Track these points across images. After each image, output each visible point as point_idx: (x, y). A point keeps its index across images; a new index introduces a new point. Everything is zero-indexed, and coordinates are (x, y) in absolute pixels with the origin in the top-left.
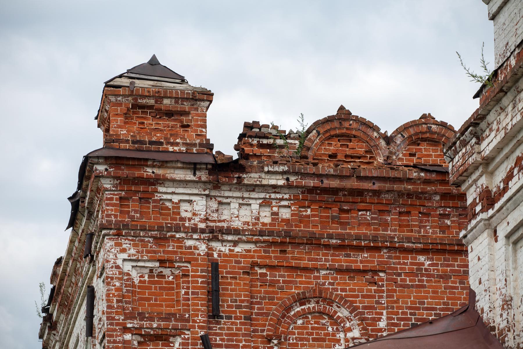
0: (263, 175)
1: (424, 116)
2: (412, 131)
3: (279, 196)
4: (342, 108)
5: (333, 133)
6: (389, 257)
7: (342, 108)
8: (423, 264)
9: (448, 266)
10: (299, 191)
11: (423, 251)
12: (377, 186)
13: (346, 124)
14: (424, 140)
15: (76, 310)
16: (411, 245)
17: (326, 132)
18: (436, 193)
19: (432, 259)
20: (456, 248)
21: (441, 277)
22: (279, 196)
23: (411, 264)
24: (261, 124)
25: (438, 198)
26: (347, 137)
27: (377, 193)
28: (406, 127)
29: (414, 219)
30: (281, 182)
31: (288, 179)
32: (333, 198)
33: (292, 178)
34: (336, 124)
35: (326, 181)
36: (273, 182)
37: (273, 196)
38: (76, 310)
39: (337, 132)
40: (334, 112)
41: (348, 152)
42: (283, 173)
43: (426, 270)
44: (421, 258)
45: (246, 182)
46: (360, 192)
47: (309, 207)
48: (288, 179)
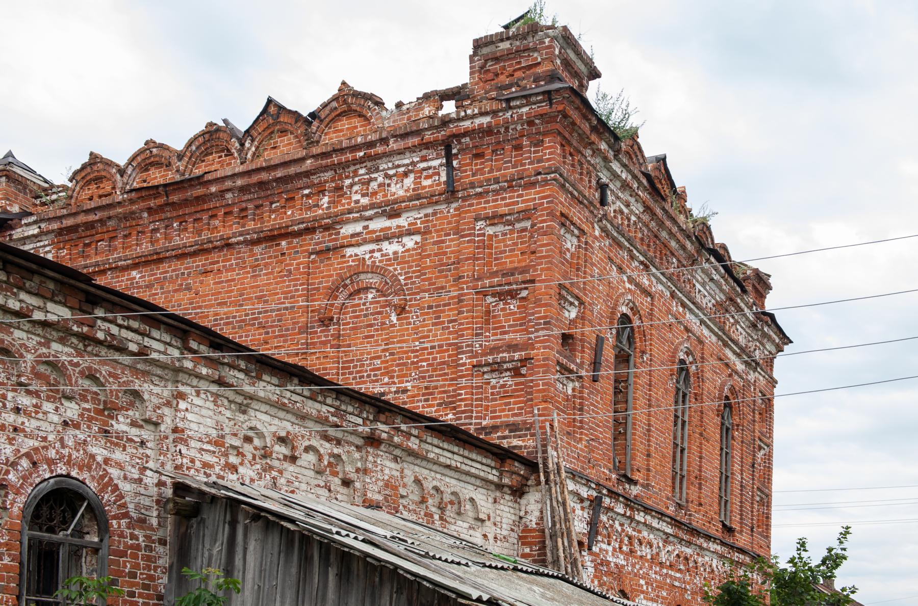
0: (24, 228)
1: (147, 143)
2: (139, 159)
3: (42, 244)
4: (91, 154)
5: (88, 178)
6: (112, 278)
7: (91, 154)
8: (135, 278)
9: (153, 275)
10: (52, 236)
11: (135, 266)
12: (99, 215)
13: (95, 168)
14: (152, 164)
15: (712, 326)
16: (123, 263)
17: (83, 178)
18: (142, 211)
19: (141, 272)
20: (155, 257)
21: (147, 286)
22: (42, 244)
23: (128, 280)
24: (639, 140)
25: (145, 215)
26: (98, 179)
27: (102, 221)
28: (134, 158)
29: (133, 240)
30: (36, 231)
31: (40, 227)
32: (74, 236)
33: (43, 225)
34: (89, 170)
35: (64, 222)
36: (31, 233)
37: (38, 244)
38: (712, 326)
39: (92, 176)
40: (86, 159)
41: (101, 192)
42: (35, 222)
43: (137, 283)
44: (134, 273)
45: (14, 237)
46: (90, 226)
47: (64, 248)
48: (40, 227)
